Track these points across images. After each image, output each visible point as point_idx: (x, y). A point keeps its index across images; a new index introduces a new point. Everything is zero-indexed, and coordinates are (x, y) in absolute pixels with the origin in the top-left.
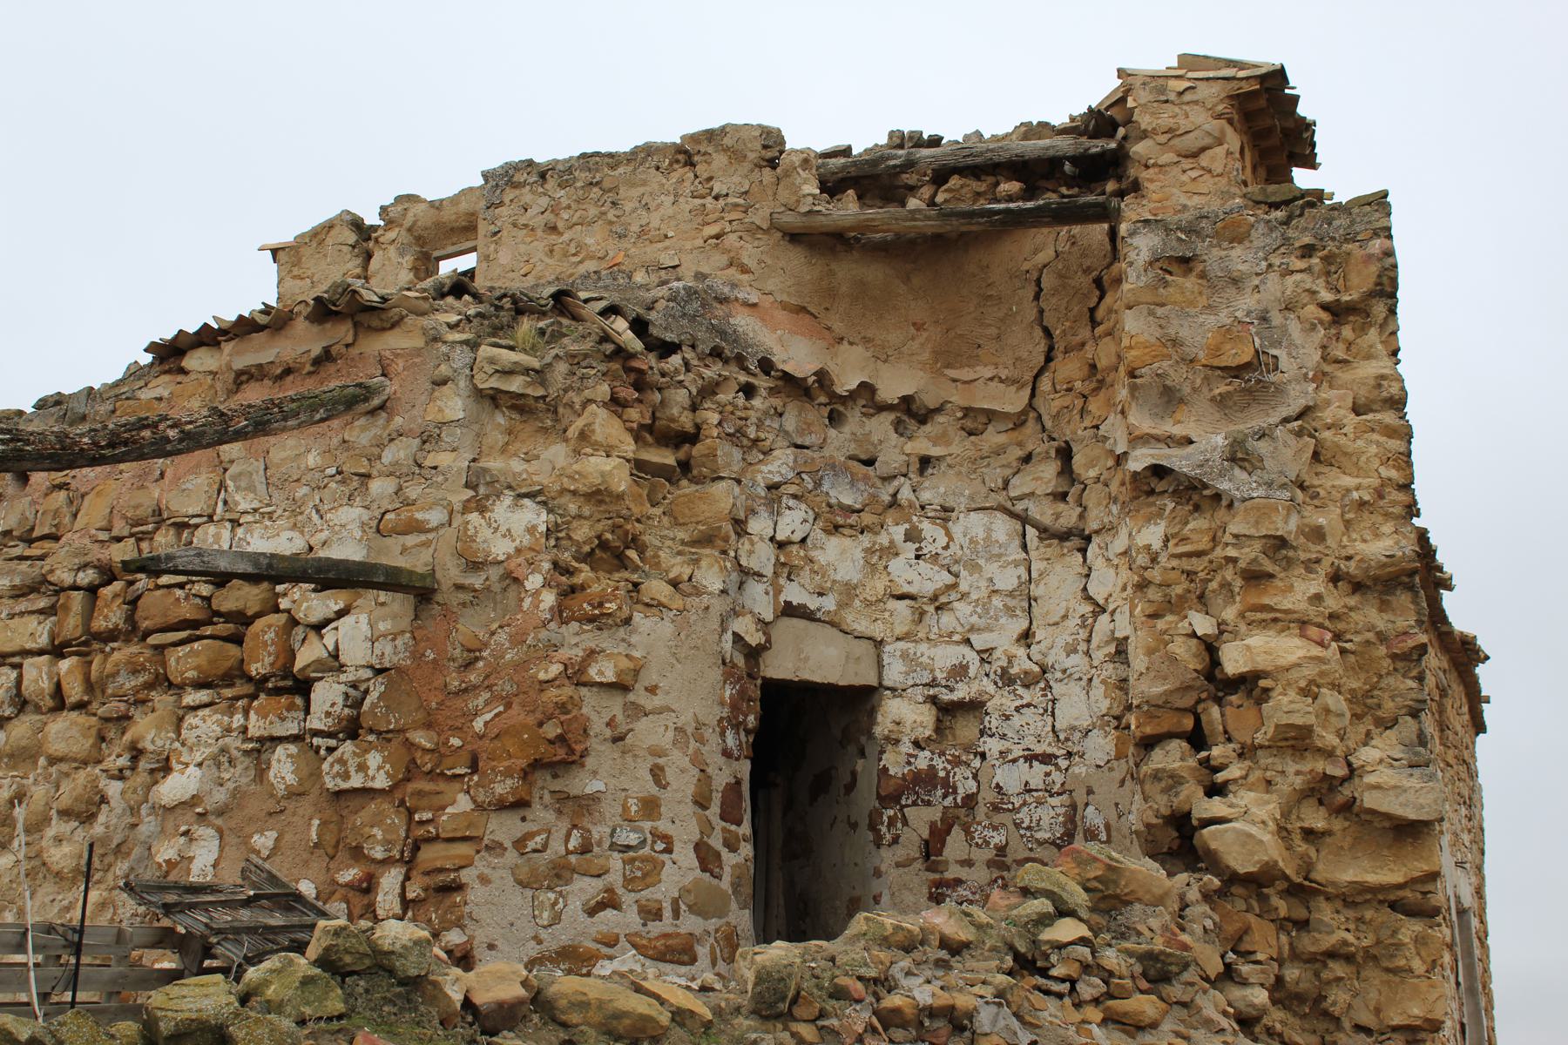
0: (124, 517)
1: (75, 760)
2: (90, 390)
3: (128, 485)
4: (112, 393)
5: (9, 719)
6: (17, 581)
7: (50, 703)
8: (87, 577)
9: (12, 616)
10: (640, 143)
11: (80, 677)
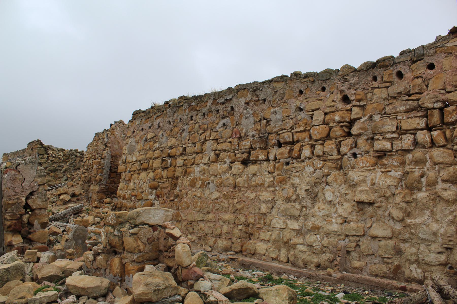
0: (451, 85)
1: (447, 164)
2: (423, 46)
3: (450, 74)
4: (433, 46)
5: (413, 150)
6: (408, 107)
7: (429, 145)
8: (440, 105)
9: (408, 118)
10: (185, 95)
11: (443, 137)
